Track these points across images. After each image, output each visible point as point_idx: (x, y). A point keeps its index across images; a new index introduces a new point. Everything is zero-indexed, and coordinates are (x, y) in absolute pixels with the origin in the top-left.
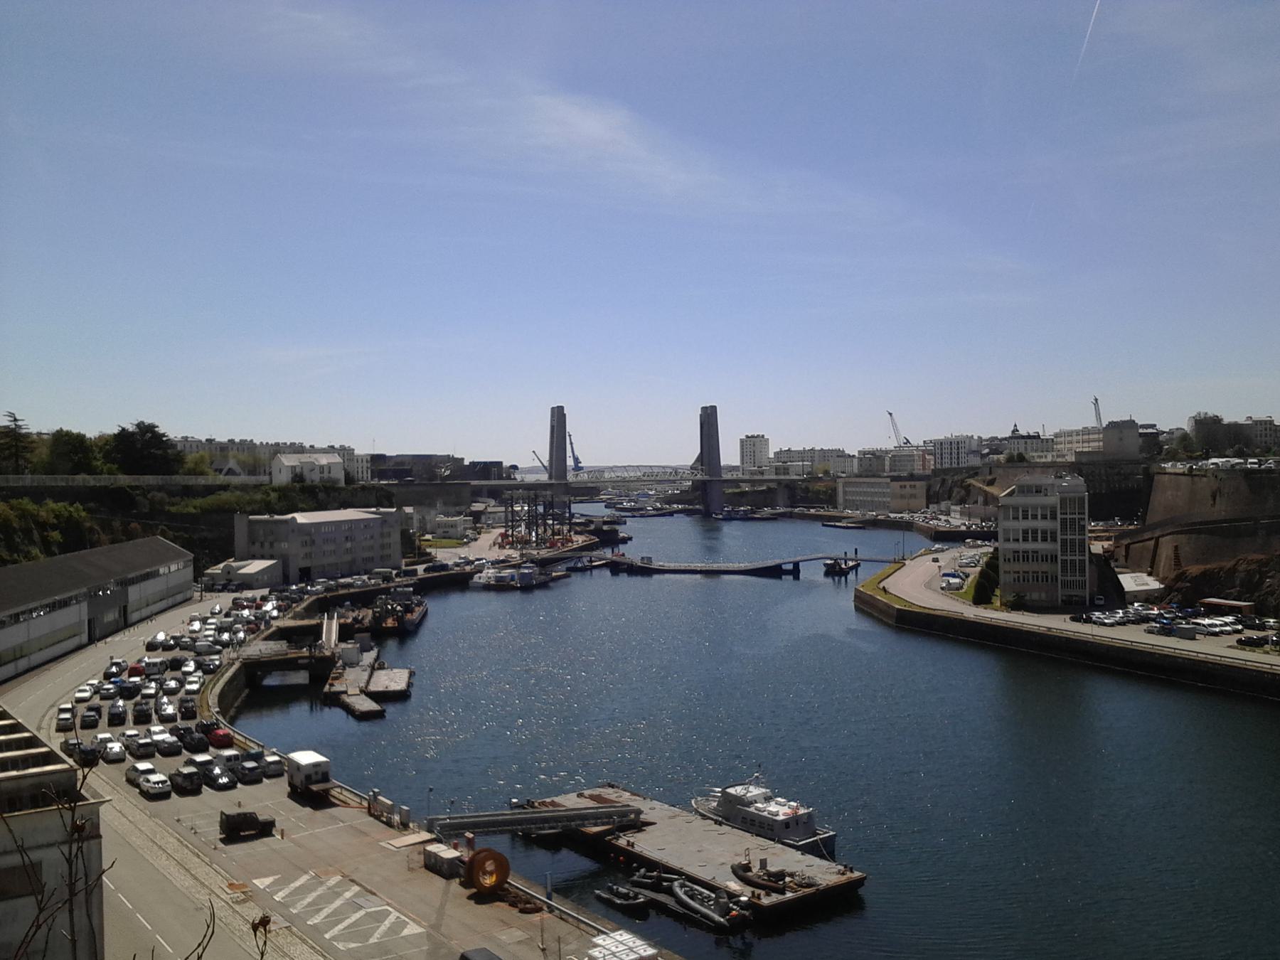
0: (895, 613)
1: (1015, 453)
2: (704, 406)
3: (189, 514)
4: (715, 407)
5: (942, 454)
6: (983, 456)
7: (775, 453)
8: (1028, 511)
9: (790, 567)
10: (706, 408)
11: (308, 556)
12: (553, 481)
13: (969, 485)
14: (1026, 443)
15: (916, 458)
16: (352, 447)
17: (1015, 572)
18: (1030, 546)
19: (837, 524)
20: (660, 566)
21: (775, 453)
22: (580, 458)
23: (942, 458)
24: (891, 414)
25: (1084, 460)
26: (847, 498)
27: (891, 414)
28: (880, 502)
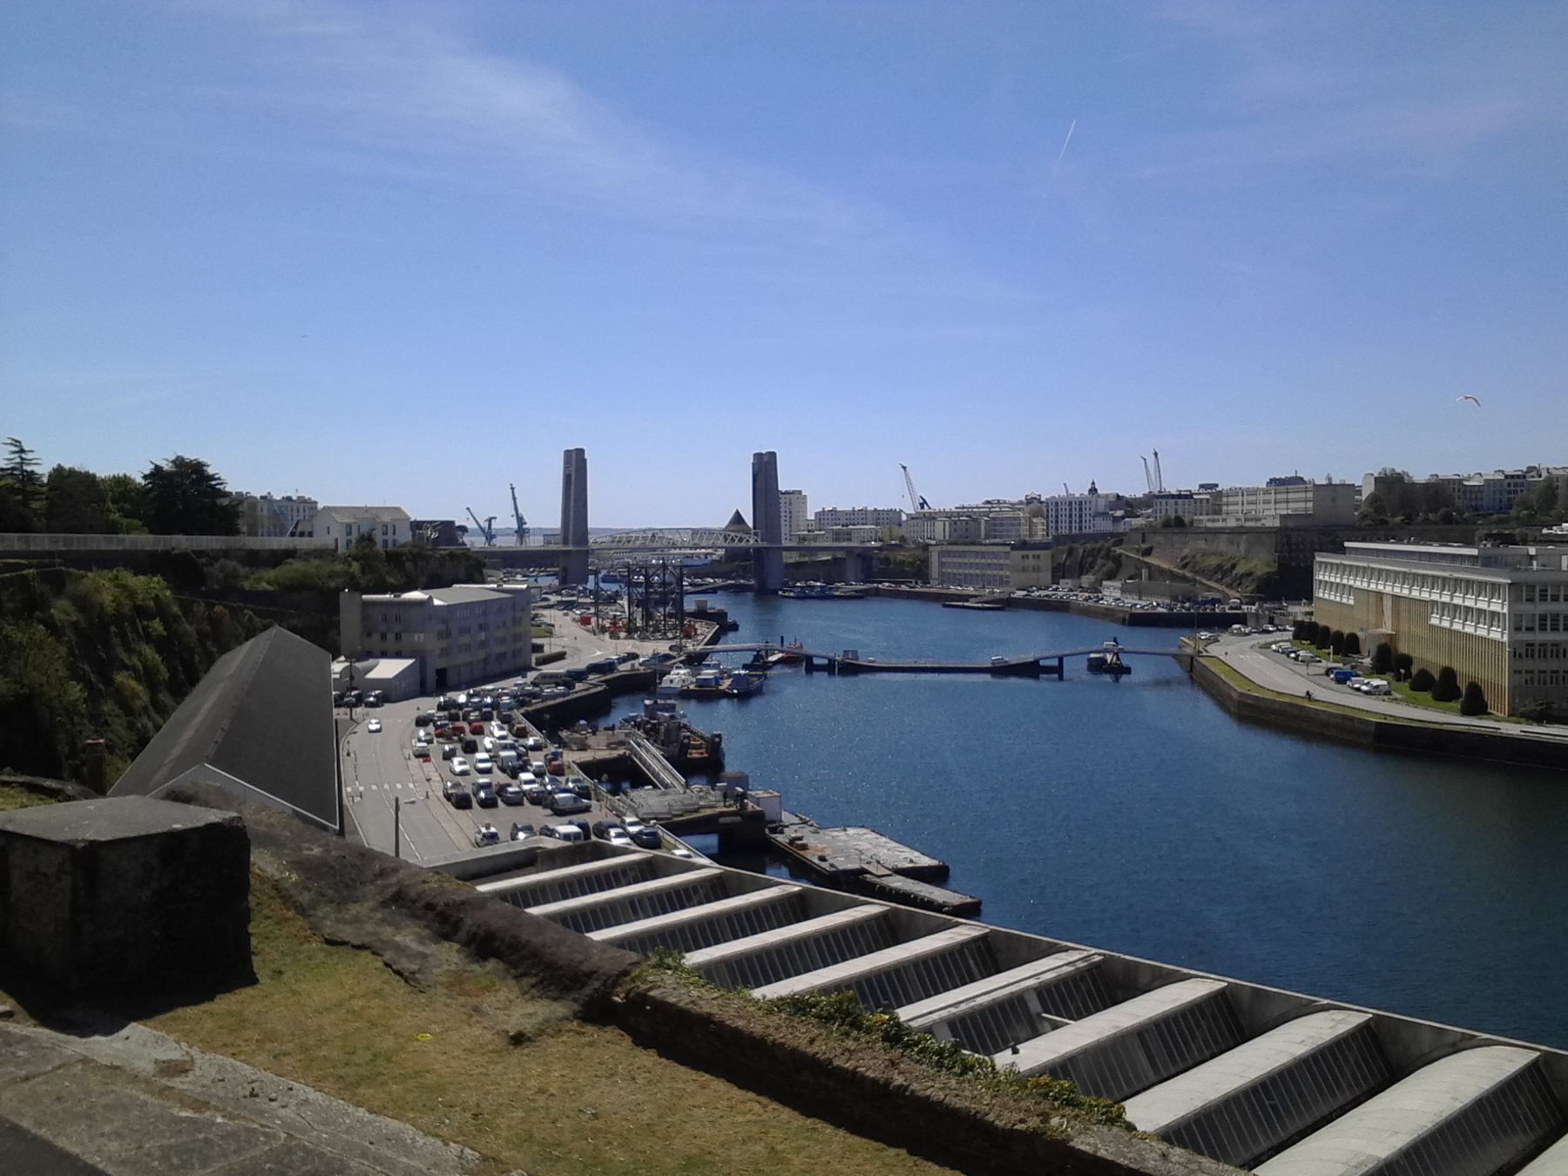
0: (1373, 728)
1: (1173, 516)
2: (758, 451)
3: (265, 592)
4: (773, 455)
5: (1057, 517)
6: (1116, 520)
7: (816, 514)
8: (1546, 591)
9: (1055, 662)
10: (761, 454)
11: (445, 652)
12: (570, 548)
13: (1120, 555)
14: (1176, 504)
15: (1023, 521)
16: (313, 499)
17: (1527, 672)
18: (1550, 637)
19: (966, 604)
20: (870, 661)
21: (816, 514)
22: (525, 517)
23: (1057, 521)
24: (904, 468)
25: (1291, 524)
26: (944, 570)
27: (904, 468)
28: (995, 576)
